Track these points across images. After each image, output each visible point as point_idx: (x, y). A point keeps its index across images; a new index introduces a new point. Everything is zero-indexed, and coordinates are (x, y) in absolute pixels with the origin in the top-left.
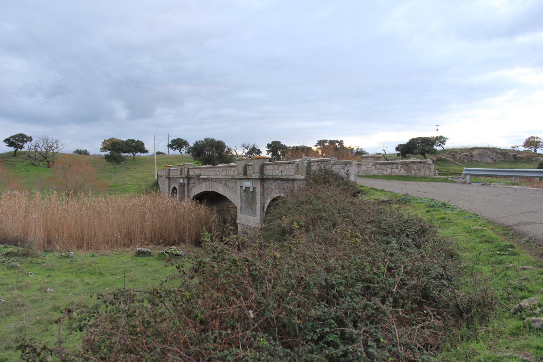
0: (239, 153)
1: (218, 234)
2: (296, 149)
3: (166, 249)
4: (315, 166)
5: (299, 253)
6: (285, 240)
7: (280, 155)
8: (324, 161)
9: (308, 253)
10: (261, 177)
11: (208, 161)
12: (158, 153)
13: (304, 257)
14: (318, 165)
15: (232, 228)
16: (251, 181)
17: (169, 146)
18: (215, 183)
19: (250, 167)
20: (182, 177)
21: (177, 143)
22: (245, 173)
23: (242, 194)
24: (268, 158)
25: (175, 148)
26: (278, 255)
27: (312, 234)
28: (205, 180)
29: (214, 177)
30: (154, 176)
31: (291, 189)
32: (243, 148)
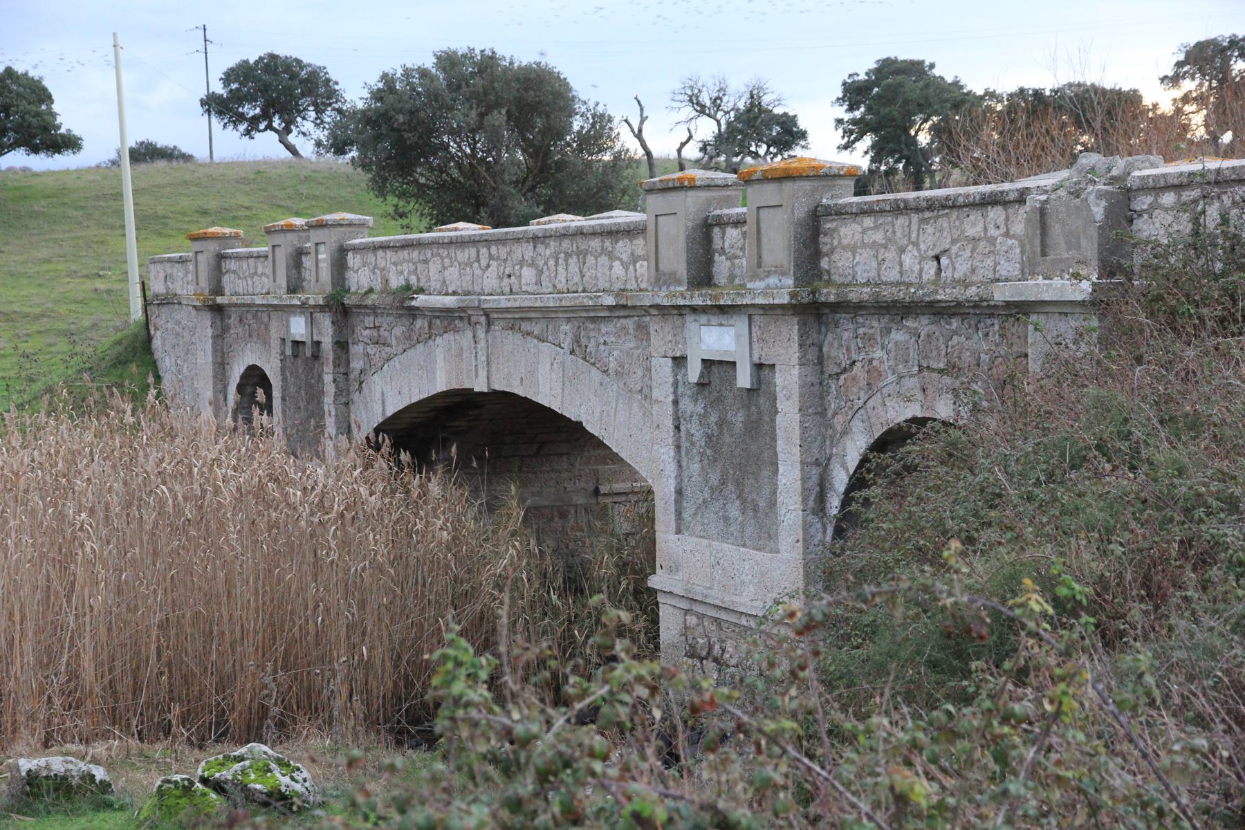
0: (663, 145)
1: (532, 655)
2: (1034, 107)
3: (204, 764)
4: (1162, 218)
5: (1059, 779)
6: (966, 699)
7: (926, 154)
8: (1221, 181)
9: (1120, 780)
10: (805, 298)
11: (469, 196)
12: (145, 154)
13: (1094, 809)
14: (1183, 206)
15: (625, 616)
16: (741, 323)
17: (215, 105)
18: (511, 342)
19: (733, 233)
20: (303, 306)
21: (265, 89)
22: (702, 276)
23: (687, 405)
24: (851, 173)
25: (254, 123)
26: (923, 791)
27: (1145, 657)
28: (449, 319)
29: (504, 302)
30: (118, 298)
31: (1000, 370)
32: (689, 111)
